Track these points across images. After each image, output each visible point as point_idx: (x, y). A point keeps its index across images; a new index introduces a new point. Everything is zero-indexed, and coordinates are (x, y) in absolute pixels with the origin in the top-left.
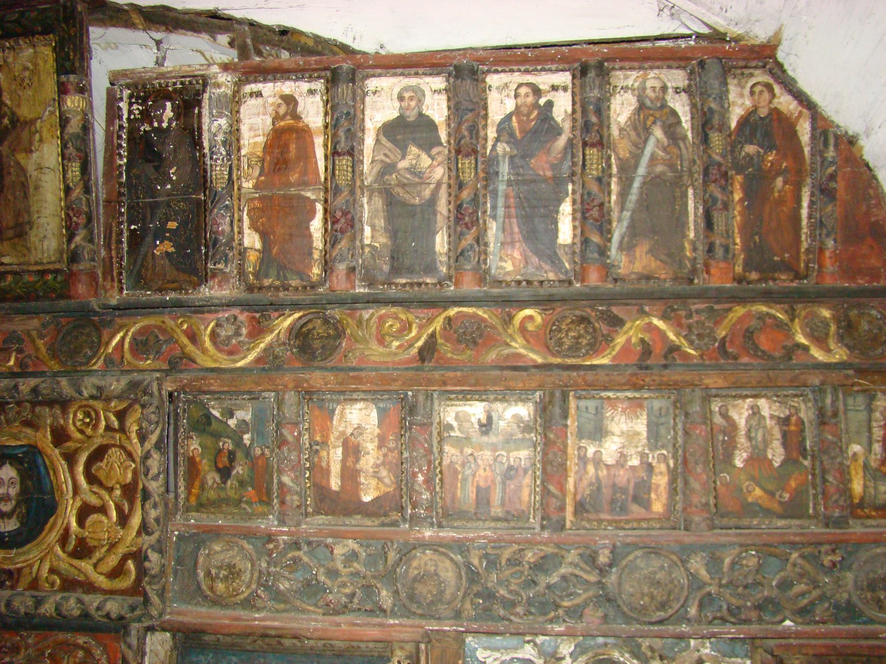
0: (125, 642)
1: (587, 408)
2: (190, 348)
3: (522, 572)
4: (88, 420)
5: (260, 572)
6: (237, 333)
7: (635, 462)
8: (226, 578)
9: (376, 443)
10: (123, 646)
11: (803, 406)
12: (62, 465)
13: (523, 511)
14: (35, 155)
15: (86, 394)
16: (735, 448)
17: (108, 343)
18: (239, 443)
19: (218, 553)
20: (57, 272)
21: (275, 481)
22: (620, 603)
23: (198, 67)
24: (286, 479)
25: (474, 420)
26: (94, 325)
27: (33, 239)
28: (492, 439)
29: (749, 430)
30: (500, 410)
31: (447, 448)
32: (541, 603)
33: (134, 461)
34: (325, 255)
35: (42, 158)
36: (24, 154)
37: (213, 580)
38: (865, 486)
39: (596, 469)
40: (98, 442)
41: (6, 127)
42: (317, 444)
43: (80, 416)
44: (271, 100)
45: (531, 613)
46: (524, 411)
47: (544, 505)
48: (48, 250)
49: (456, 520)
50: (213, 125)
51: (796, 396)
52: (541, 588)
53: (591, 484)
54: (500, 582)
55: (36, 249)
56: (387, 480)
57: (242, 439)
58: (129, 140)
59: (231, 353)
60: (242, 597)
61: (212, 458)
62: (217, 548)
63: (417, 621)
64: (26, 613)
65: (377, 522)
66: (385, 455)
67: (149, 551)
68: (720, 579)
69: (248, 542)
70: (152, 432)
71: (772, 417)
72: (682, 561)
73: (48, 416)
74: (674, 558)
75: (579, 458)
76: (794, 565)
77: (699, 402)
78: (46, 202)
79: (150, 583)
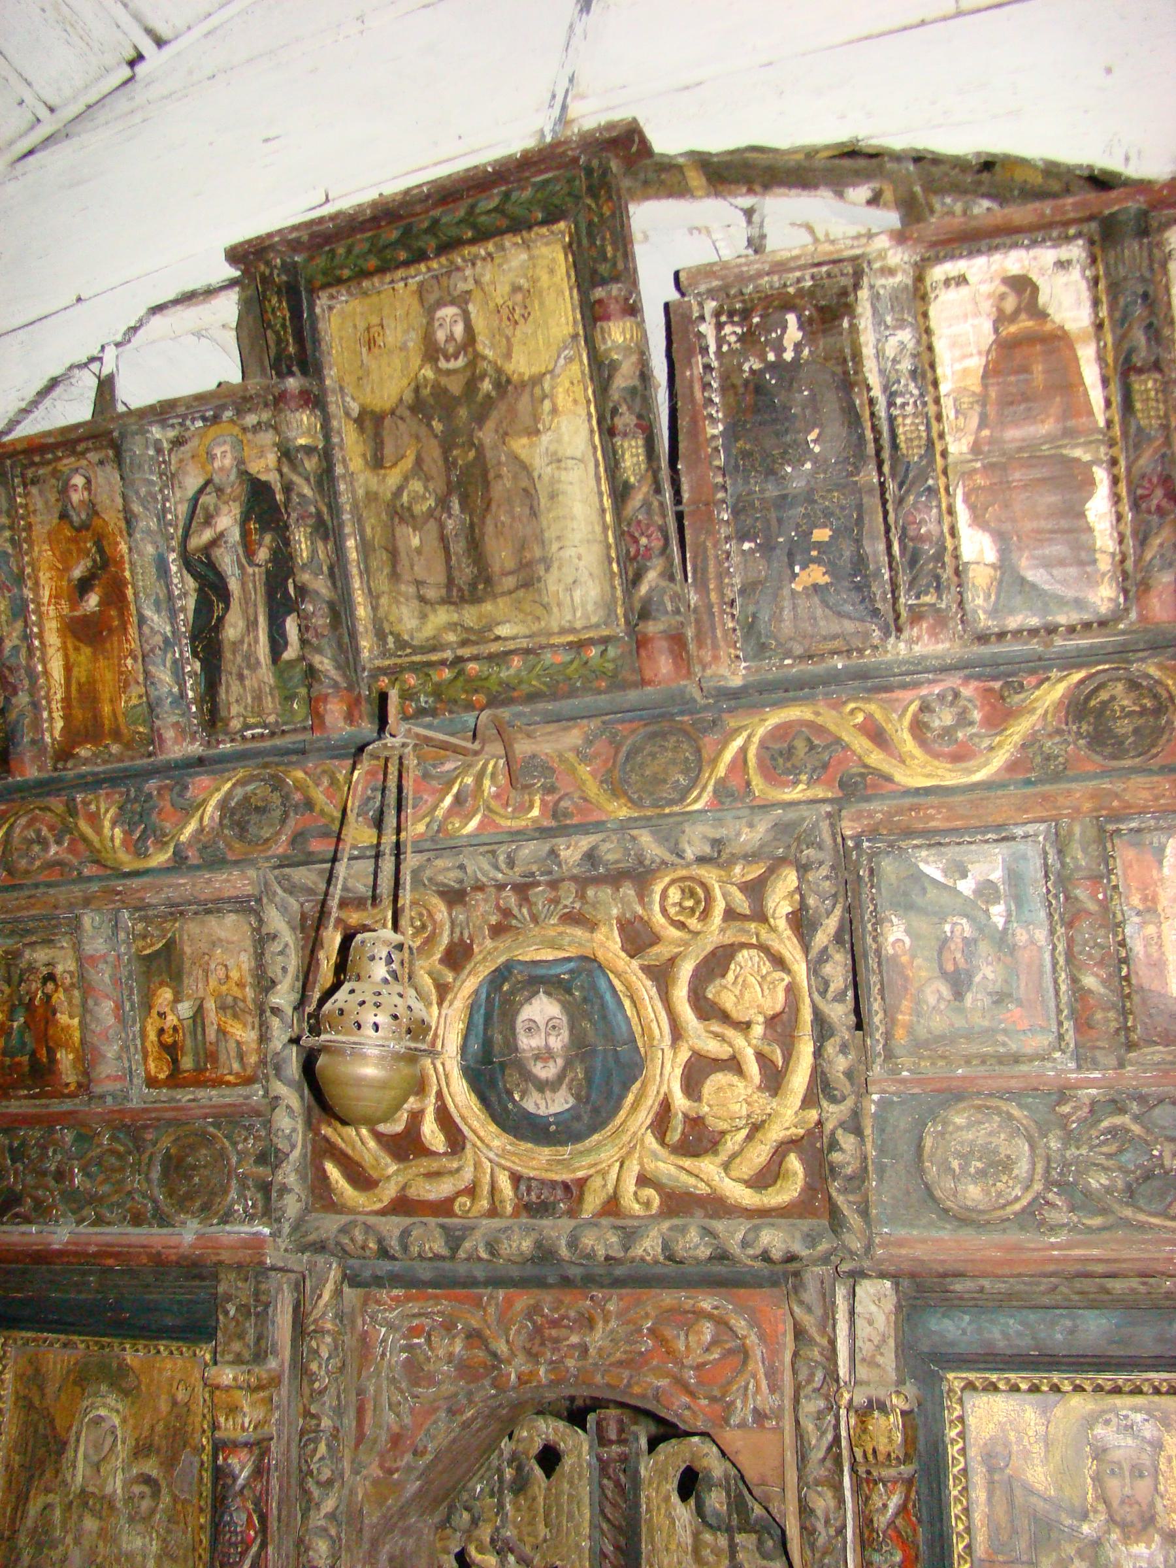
0: (801, 1303)
2: (876, 758)
5: (1048, 1160)
6: (963, 720)
8: (982, 1173)
12: (646, 989)
14: (545, 439)
15: (690, 854)
17: (714, 761)
18: (983, 927)
20: (605, 641)
23: (849, 242)
26: (686, 733)
27: (552, 588)
34: (1122, 561)
35: (559, 441)
36: (524, 441)
41: (488, 396)
43: (674, 895)
44: (986, 288)
48: (583, 605)
50: (880, 344)
55: (559, 605)
58: (723, 390)
59: (957, 758)
60: (1017, 1207)
62: (959, 1120)
64: (608, 1258)
67: (840, 1131)
69: (1020, 1106)
70: (829, 914)
73: (612, 904)
78: (573, 518)
79: (844, 1191)
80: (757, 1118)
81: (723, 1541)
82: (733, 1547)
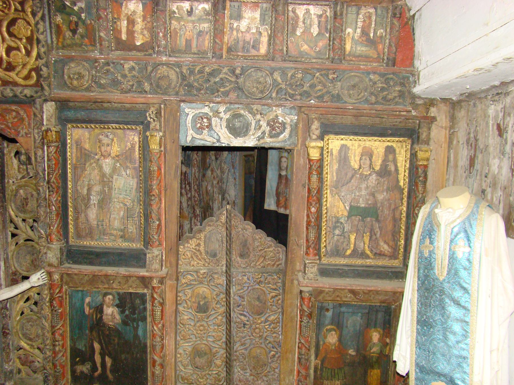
0: (34, 107)
1: (234, 6)
3: (204, 76)
4: (5, 6)
7: (254, 31)
8: (77, 79)
9: (142, 19)
10: (34, 109)
11: (329, 10)
13: (205, 51)
16: (297, 27)
18: (80, 18)
19: (73, 68)
21: (97, 35)
22: (244, 90)
24: (102, 34)
25: (185, 9)
28: (193, 18)
29: (304, 20)
30: (196, 5)
31: (173, 22)
32: (212, 89)
33: (31, 26)
37: (72, 79)
38: (352, 47)
39: (237, 33)
40: (12, 16)
42: (116, 19)
45: (207, 93)
46: (207, 6)
47: (214, 48)
49: (177, 53)
51: (326, 5)
52: (212, 83)
53: (235, 40)
54: (195, 80)
56: (147, 36)
57: (81, 16)
60: (85, 87)
61: (68, 25)
62: (73, 65)
63: (160, 96)
65: (143, 54)
66: (146, 25)
67: (42, 67)
68: (286, 82)
70: (39, 12)
71: (315, 14)
72: (271, 74)
74: (267, 72)
75: (230, 28)
76: (317, 78)
77: (281, 5)
79: (44, 81)
80: (24, 63)
81: (25, 167)
82: (27, 168)
